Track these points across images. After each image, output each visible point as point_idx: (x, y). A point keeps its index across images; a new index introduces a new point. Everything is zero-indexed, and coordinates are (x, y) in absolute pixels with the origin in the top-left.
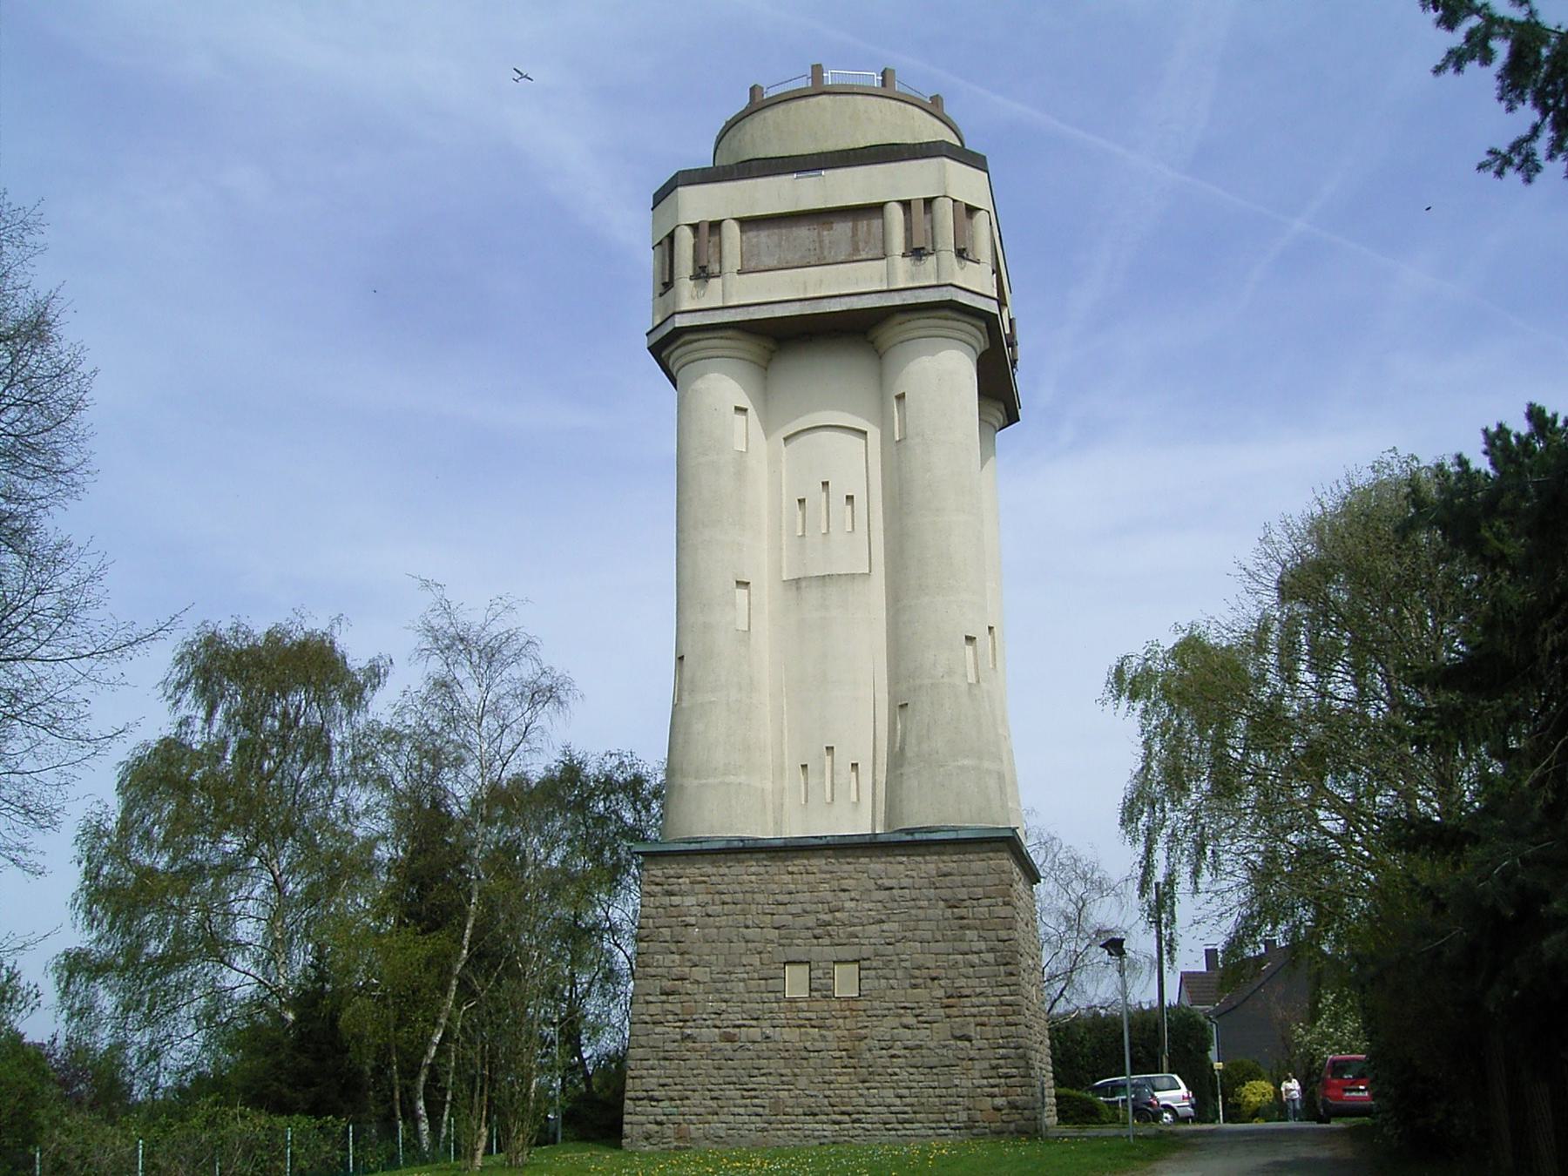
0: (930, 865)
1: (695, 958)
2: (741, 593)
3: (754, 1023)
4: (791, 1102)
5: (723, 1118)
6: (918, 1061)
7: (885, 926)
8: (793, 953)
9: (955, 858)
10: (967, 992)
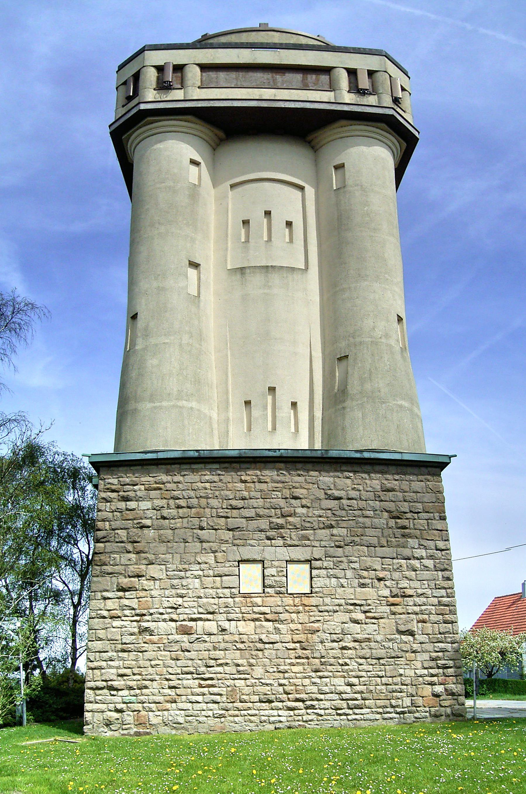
0: (375, 481)
1: (151, 557)
2: (192, 273)
3: (210, 617)
4: (246, 690)
5: (181, 705)
6: (366, 652)
7: (335, 531)
8: (247, 553)
9: (397, 477)
10: (409, 592)
